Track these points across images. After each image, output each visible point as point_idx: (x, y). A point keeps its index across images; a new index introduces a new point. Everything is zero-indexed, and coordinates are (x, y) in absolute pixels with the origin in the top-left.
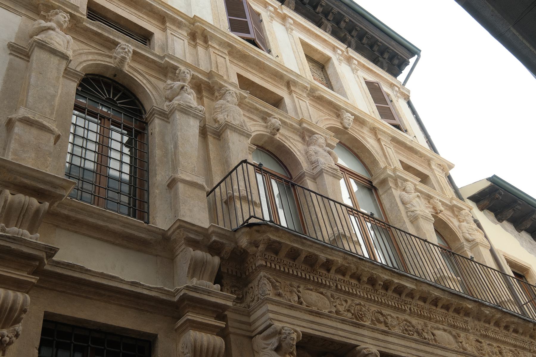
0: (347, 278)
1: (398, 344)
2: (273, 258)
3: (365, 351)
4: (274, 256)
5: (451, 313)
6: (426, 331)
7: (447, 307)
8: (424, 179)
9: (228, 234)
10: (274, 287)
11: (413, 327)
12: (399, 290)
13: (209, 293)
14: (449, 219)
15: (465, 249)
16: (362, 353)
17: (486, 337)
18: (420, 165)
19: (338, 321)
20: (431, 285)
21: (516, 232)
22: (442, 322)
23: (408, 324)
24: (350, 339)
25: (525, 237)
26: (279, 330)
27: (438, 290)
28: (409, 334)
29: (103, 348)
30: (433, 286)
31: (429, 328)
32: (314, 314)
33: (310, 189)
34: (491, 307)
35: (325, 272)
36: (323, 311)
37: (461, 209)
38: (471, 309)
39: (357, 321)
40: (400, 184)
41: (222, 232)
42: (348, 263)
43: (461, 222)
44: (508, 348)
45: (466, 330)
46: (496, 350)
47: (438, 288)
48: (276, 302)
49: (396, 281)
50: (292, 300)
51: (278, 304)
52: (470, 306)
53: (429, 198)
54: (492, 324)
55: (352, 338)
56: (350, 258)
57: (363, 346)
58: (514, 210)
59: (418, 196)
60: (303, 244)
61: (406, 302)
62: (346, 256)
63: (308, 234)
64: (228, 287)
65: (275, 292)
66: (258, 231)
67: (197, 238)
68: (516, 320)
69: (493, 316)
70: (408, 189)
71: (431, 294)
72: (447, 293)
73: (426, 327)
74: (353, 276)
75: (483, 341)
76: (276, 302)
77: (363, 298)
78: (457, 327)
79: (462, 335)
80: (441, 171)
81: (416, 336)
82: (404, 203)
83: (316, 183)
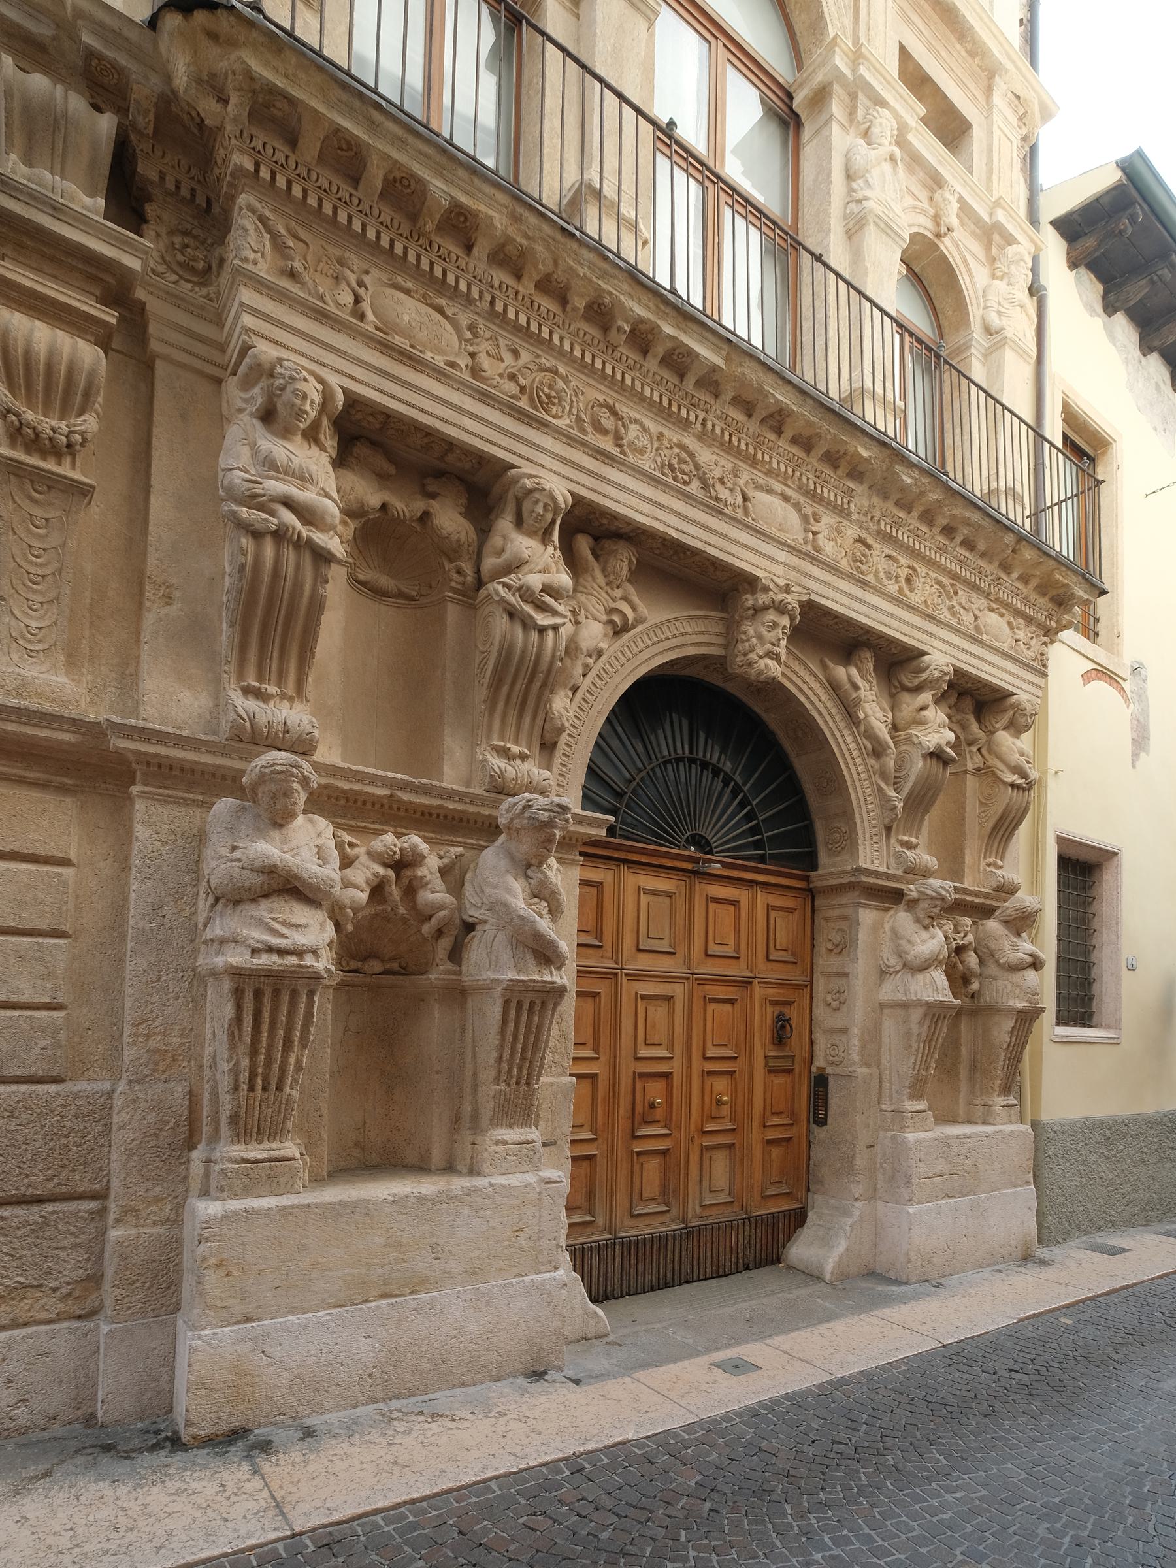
0: (527, 287)
1: (633, 491)
2: (280, 157)
3: (528, 483)
4: (287, 150)
6: (729, 485)
7: (805, 443)
8: (951, 128)
9: (133, 35)
10: (279, 247)
11: (697, 466)
12: (678, 362)
13: (54, 208)
14: (966, 263)
15: (973, 350)
16: (520, 485)
17: (888, 538)
18: (961, 84)
19: (467, 391)
20: (770, 369)
21: (1137, 353)
22: (784, 479)
23: (684, 455)
24: (828, 599)
25: (1152, 370)
26: (267, 366)
27: (789, 388)
28: (675, 479)
30: (777, 373)
31: (741, 482)
32: (396, 356)
33: (549, 30)
34: (923, 470)
35: (457, 251)
36: (428, 355)
37: (1010, 240)
38: (867, 460)
39: (532, 409)
40: (860, 113)
42: (528, 238)
43: (997, 279)
44: (934, 575)
45: (842, 512)
46: (903, 573)
47: (790, 382)
49: (668, 329)
50: (328, 298)
51: (280, 296)
52: (865, 453)
53: (935, 182)
54: (915, 514)
55: (502, 443)
56: (533, 220)
57: (527, 468)
58: (1152, 282)
59: (892, 158)
61: (695, 401)
62: (520, 210)
63: (798, 372)
64: (163, 231)
65: (281, 263)
66: (213, 36)
68: (975, 517)
69: (922, 494)
70: (875, 130)
71: (766, 395)
72: (811, 402)
73: (736, 476)
74: (544, 285)
75: (875, 545)
77: (569, 359)
78: (822, 499)
79: (828, 519)
80: (1013, 119)
81: (694, 488)
82: (849, 177)
83: (578, 16)
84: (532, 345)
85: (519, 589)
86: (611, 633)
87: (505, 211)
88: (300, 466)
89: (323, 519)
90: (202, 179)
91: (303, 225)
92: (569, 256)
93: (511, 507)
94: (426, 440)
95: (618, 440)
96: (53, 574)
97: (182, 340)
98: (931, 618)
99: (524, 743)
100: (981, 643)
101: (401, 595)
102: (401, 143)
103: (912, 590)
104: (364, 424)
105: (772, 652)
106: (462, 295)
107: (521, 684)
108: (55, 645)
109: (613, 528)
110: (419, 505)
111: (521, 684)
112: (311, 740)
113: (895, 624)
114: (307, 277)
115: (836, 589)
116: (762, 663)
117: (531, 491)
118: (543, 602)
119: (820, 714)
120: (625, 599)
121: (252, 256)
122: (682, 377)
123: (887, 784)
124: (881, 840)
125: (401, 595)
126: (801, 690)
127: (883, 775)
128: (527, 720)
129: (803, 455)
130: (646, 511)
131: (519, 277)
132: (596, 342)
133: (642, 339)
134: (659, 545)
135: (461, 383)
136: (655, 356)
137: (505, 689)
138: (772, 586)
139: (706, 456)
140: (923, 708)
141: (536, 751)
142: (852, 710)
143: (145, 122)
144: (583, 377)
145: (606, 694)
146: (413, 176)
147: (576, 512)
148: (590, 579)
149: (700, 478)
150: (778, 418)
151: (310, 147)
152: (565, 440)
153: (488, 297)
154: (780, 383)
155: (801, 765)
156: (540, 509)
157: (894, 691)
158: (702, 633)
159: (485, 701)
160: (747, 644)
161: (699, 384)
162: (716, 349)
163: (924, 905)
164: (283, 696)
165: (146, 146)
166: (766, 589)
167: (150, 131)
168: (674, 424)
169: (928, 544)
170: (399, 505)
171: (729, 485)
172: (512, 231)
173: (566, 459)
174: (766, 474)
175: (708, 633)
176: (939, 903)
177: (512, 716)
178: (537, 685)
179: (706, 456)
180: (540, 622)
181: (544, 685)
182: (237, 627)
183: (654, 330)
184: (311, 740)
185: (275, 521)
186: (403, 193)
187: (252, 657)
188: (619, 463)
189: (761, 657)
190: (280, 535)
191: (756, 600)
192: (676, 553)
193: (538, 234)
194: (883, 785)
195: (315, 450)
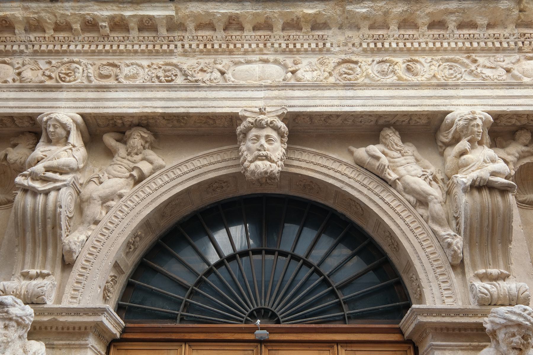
1: (125, 99)
3: (45, 119)
5: (278, 32)
6: (209, 70)
11: (181, 70)
28: (160, 82)
42: (36, 13)
54: (393, 27)
69: (386, 14)
71: (213, 15)
74: (58, 28)
81: (180, 80)
85: (30, 175)
86: (132, 182)
87: (20, 9)
98: (444, 86)
99: (501, 263)
100: (521, 85)
103: (416, 75)
105: (259, 156)
107: (39, 229)
111: (39, 229)
113: (399, 102)
115: (178, 99)
116: (252, 166)
117: (46, 122)
119: (353, 187)
120: (144, 159)
122: (156, 30)
123: (441, 225)
124: (449, 278)
126: (327, 175)
127: (436, 220)
128: (50, 251)
129: (269, 33)
130: (137, 106)
131: (44, 31)
135: (7, 87)
136: (133, 29)
137: (29, 235)
138: (247, 114)
140: (463, 153)
142: (382, 176)
144: (96, 57)
152: (75, 90)
155: (370, 230)
157: (441, 150)
158: (219, 162)
163: (501, 336)
166: (245, 118)
168: (162, 55)
169: (421, 40)
171: (209, 70)
172: (27, 14)
173: (76, 99)
174: (244, 54)
176: (515, 330)
178: (49, 226)
179: (187, 63)
188: (114, 88)
189: (251, 162)
194: (436, 228)
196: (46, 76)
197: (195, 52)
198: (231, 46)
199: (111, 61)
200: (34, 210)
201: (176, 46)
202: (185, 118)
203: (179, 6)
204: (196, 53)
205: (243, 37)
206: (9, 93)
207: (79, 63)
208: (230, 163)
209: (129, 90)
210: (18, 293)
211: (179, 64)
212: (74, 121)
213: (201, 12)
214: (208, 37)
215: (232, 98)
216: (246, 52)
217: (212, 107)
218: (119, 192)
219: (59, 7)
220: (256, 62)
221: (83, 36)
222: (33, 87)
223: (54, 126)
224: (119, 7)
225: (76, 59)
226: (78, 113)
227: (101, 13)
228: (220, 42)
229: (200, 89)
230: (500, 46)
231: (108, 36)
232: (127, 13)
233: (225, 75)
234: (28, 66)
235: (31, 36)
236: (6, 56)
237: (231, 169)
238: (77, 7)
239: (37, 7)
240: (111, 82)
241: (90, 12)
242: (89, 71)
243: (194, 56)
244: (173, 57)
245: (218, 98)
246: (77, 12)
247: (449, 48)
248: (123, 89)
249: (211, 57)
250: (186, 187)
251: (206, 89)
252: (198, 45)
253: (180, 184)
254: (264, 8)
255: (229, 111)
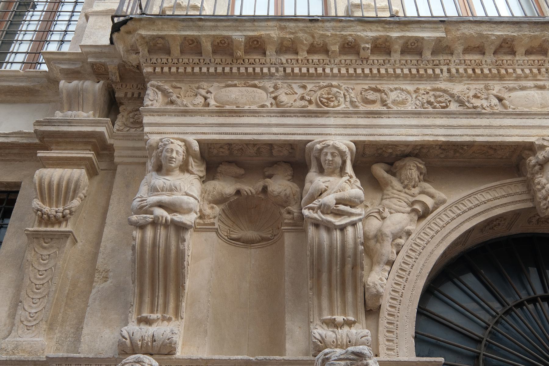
0: (303, 55)
1: (401, 125)
2: (164, 61)
3: (319, 146)
4: (167, 57)
6: (483, 97)
9: (106, 50)
11: (452, 96)
12: (413, 48)
13: (69, 122)
26: (155, 145)
27: (503, 26)
28: (434, 107)
29: (3, 209)
32: (227, 114)
36: (247, 107)
39: (320, 109)
41: (97, 50)
48: (157, 112)
49: (395, 34)
56: (292, 25)
57: (317, 139)
60: (200, 28)
62: (283, 24)
66: (129, 33)
67: (73, 67)
71: (487, 37)
72: (527, 25)
74: (312, 50)
76: (157, 112)
77: (340, 76)
81: (454, 107)
84: (315, 80)
85: (319, 207)
86: (416, 218)
87: (276, 28)
88: (170, 185)
89: (181, 206)
90: (143, 87)
91: (179, 82)
92: (319, 30)
93: (314, 164)
94: (255, 149)
95: (384, 103)
96: (48, 281)
97: (130, 153)
101: (263, 239)
102: (215, 28)
104: (221, 154)
106: (266, 74)
107: (336, 270)
108: (42, 320)
109: (399, 153)
110: (260, 184)
112: (170, 343)
114: (179, 101)
117: (321, 150)
118: (338, 210)
120: (422, 192)
121: (151, 103)
122: (420, 54)
125: (263, 239)
128: (350, 295)
130: (415, 133)
131: (297, 53)
132: (354, 61)
133: (382, 47)
134: (440, 151)
135: (268, 112)
137: (325, 276)
139: (457, 88)
141: (362, 316)
143: (115, 77)
145: (421, 261)
146: (225, 37)
147: (367, 152)
148: (390, 188)
149: (457, 101)
150: (507, 45)
151: (176, 50)
152: (343, 115)
153: (281, 69)
154: (494, 26)
156: (329, 157)
158: (504, 196)
159: (311, 289)
160: (544, 191)
161: (434, 53)
162: (436, 29)
164: (164, 319)
165: (119, 86)
167: (118, 79)
168: (426, 80)
170: (247, 188)
171: (483, 97)
172: (283, 35)
173: (346, 125)
175: (509, 195)
177: (337, 295)
178: (349, 267)
179: (457, 88)
180: (338, 223)
181: (354, 267)
182: (136, 283)
183: (387, 39)
184: (170, 343)
185: (152, 216)
186: (223, 47)
187: (147, 299)
188: (386, 114)
190: (155, 223)
191: (537, 157)
192: (456, 151)
193: (297, 29)
195: (187, 175)
196: (306, 100)
197: (462, 77)
198: (503, 71)
199: (374, 86)
200: (331, 246)
201: (442, 70)
202: (465, 147)
203: (450, 28)
204: (464, 79)
205: (515, 61)
206: (269, 118)
207: (339, 87)
208: (517, 198)
209: (403, 116)
210: (339, 343)
211: (449, 89)
212: (350, 149)
213: (474, 34)
214: (477, 61)
215: (520, 126)
216: (518, 78)
217: (500, 135)
218: (406, 228)
219: (319, 26)
220: (530, 88)
221: (340, 59)
222: (297, 113)
223: (333, 154)
224: (384, 28)
225: (334, 83)
226: (351, 141)
227: (365, 33)
228: (490, 67)
229: (481, 116)
230: (314, 72)
231: (367, 59)
232: (363, 34)
233: (504, 101)
234: (283, 90)
235: (282, 58)
236: (255, 79)
237: (518, 205)
238: (339, 27)
239: (294, 27)
240: (377, 107)
241: (353, 33)
242: (352, 95)
243: (460, 82)
244: (438, 82)
245: (504, 126)
246: (338, 33)
247: (523, 75)
248: (396, 116)
249: (479, 82)
250: (474, 224)
251: (488, 116)
252: (465, 70)
253: (467, 220)
254: (542, 31)
255: (520, 140)
